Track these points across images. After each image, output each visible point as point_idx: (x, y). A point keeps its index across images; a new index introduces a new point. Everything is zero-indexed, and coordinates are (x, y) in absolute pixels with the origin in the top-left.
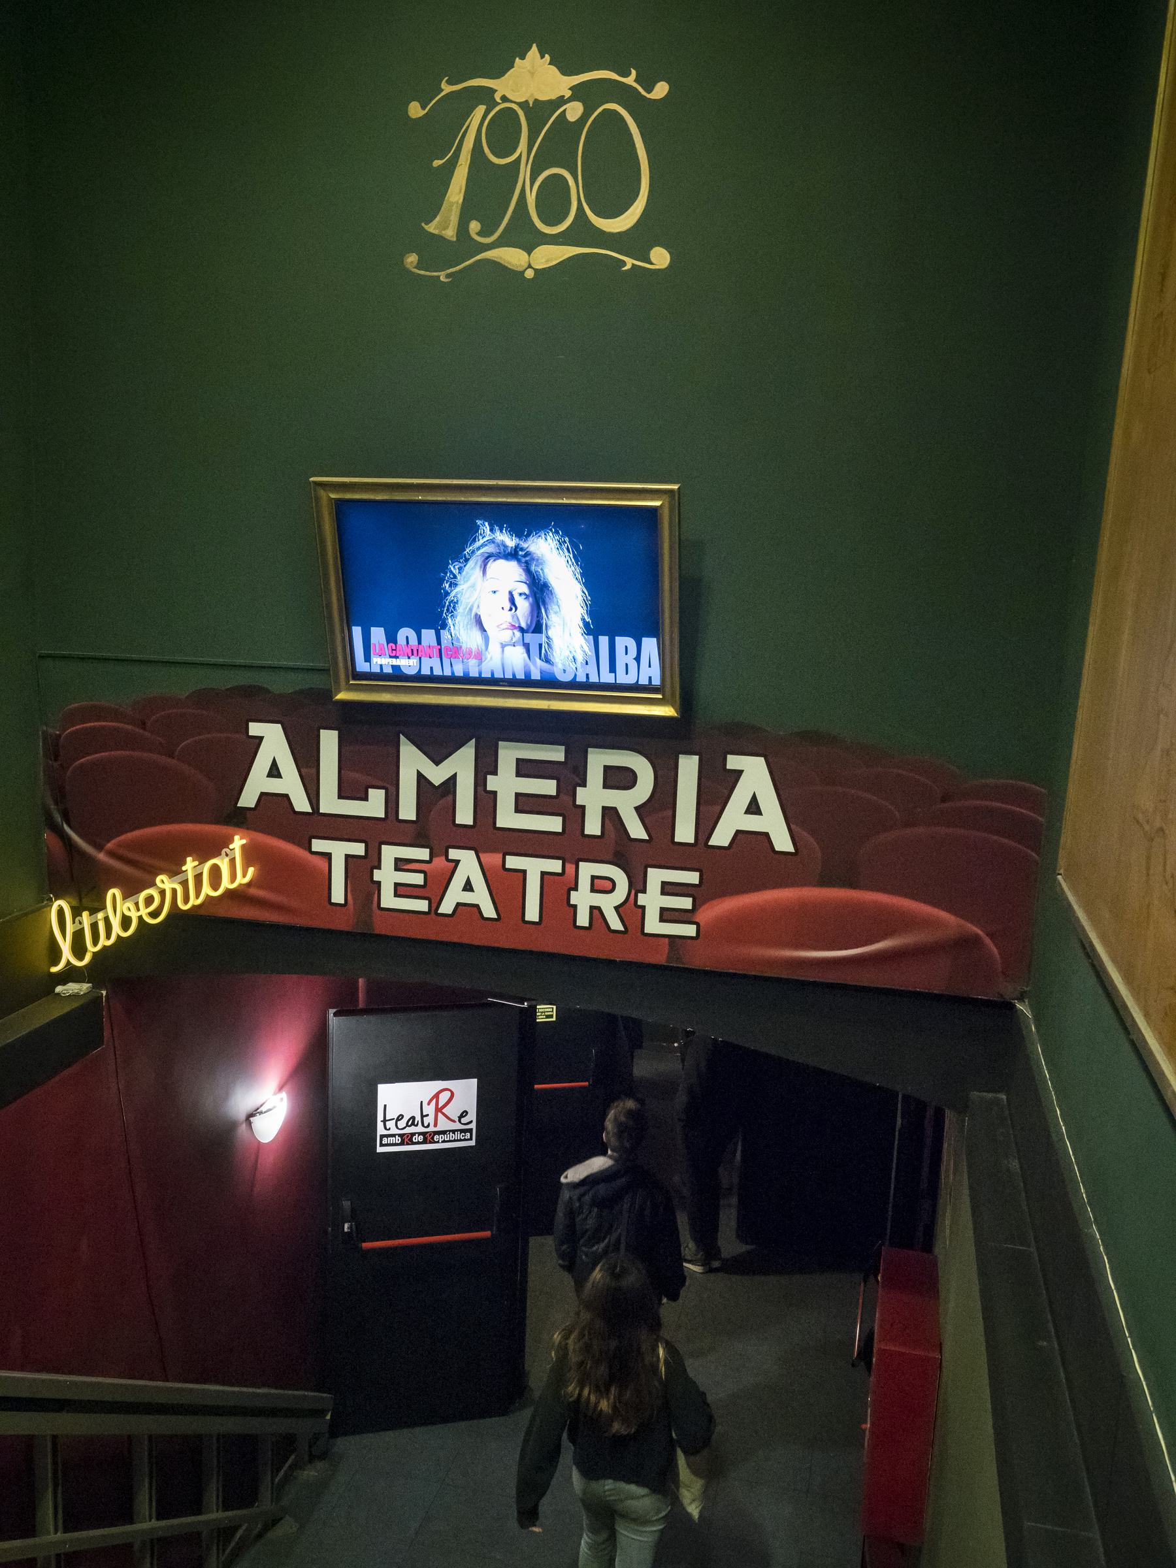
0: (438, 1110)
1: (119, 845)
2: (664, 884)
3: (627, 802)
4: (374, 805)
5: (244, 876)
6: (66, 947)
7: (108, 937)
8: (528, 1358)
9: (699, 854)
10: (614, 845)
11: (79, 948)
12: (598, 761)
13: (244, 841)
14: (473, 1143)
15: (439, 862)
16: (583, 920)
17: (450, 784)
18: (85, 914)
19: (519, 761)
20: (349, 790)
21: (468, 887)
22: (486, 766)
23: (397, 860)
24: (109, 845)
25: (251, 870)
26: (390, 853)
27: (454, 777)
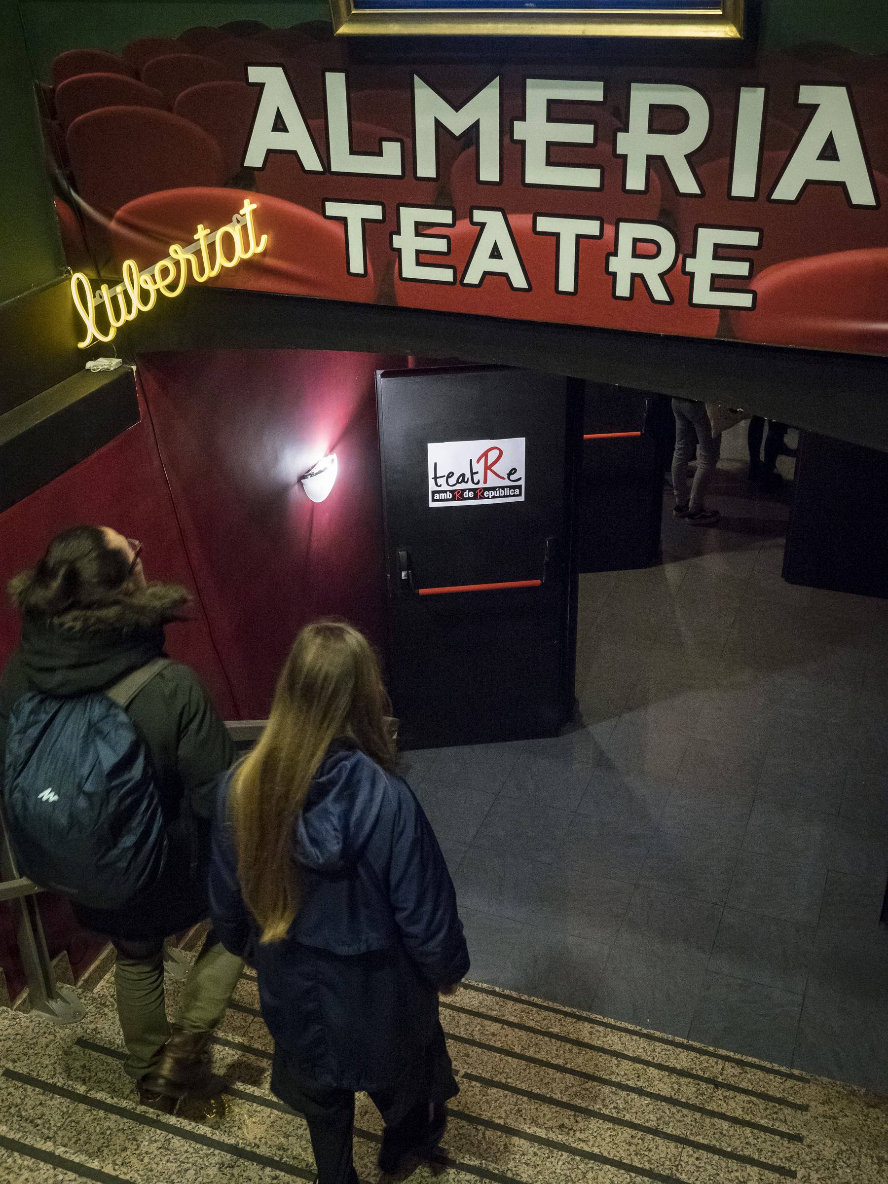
0: (487, 468)
1: (132, 212)
2: (717, 246)
3: (675, 149)
4: (388, 162)
5: (258, 244)
6: (89, 320)
7: (129, 311)
8: (578, 686)
9: (758, 211)
10: (661, 203)
11: (103, 324)
12: (643, 98)
13: (254, 206)
14: (522, 498)
15: (463, 225)
16: (623, 289)
17: (474, 130)
18: (104, 287)
19: (550, 102)
20: (361, 145)
21: (496, 254)
22: (512, 110)
23: (418, 224)
24: (119, 213)
25: (264, 238)
26: (409, 216)
27: (476, 125)
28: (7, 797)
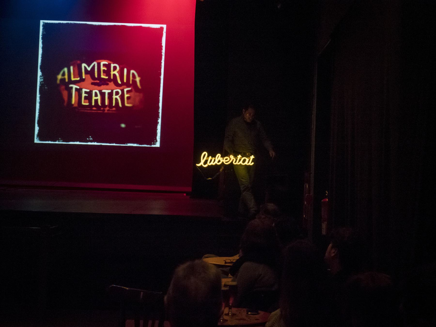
11: (205, 163)
25: (253, 163)
28: (114, 112)
